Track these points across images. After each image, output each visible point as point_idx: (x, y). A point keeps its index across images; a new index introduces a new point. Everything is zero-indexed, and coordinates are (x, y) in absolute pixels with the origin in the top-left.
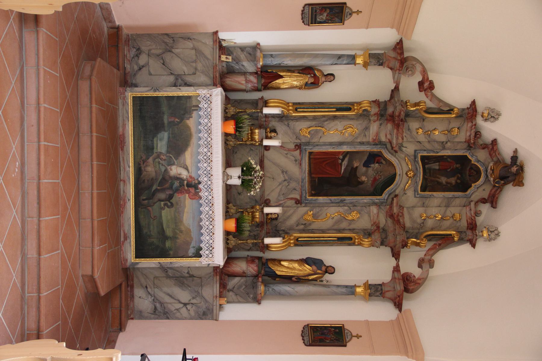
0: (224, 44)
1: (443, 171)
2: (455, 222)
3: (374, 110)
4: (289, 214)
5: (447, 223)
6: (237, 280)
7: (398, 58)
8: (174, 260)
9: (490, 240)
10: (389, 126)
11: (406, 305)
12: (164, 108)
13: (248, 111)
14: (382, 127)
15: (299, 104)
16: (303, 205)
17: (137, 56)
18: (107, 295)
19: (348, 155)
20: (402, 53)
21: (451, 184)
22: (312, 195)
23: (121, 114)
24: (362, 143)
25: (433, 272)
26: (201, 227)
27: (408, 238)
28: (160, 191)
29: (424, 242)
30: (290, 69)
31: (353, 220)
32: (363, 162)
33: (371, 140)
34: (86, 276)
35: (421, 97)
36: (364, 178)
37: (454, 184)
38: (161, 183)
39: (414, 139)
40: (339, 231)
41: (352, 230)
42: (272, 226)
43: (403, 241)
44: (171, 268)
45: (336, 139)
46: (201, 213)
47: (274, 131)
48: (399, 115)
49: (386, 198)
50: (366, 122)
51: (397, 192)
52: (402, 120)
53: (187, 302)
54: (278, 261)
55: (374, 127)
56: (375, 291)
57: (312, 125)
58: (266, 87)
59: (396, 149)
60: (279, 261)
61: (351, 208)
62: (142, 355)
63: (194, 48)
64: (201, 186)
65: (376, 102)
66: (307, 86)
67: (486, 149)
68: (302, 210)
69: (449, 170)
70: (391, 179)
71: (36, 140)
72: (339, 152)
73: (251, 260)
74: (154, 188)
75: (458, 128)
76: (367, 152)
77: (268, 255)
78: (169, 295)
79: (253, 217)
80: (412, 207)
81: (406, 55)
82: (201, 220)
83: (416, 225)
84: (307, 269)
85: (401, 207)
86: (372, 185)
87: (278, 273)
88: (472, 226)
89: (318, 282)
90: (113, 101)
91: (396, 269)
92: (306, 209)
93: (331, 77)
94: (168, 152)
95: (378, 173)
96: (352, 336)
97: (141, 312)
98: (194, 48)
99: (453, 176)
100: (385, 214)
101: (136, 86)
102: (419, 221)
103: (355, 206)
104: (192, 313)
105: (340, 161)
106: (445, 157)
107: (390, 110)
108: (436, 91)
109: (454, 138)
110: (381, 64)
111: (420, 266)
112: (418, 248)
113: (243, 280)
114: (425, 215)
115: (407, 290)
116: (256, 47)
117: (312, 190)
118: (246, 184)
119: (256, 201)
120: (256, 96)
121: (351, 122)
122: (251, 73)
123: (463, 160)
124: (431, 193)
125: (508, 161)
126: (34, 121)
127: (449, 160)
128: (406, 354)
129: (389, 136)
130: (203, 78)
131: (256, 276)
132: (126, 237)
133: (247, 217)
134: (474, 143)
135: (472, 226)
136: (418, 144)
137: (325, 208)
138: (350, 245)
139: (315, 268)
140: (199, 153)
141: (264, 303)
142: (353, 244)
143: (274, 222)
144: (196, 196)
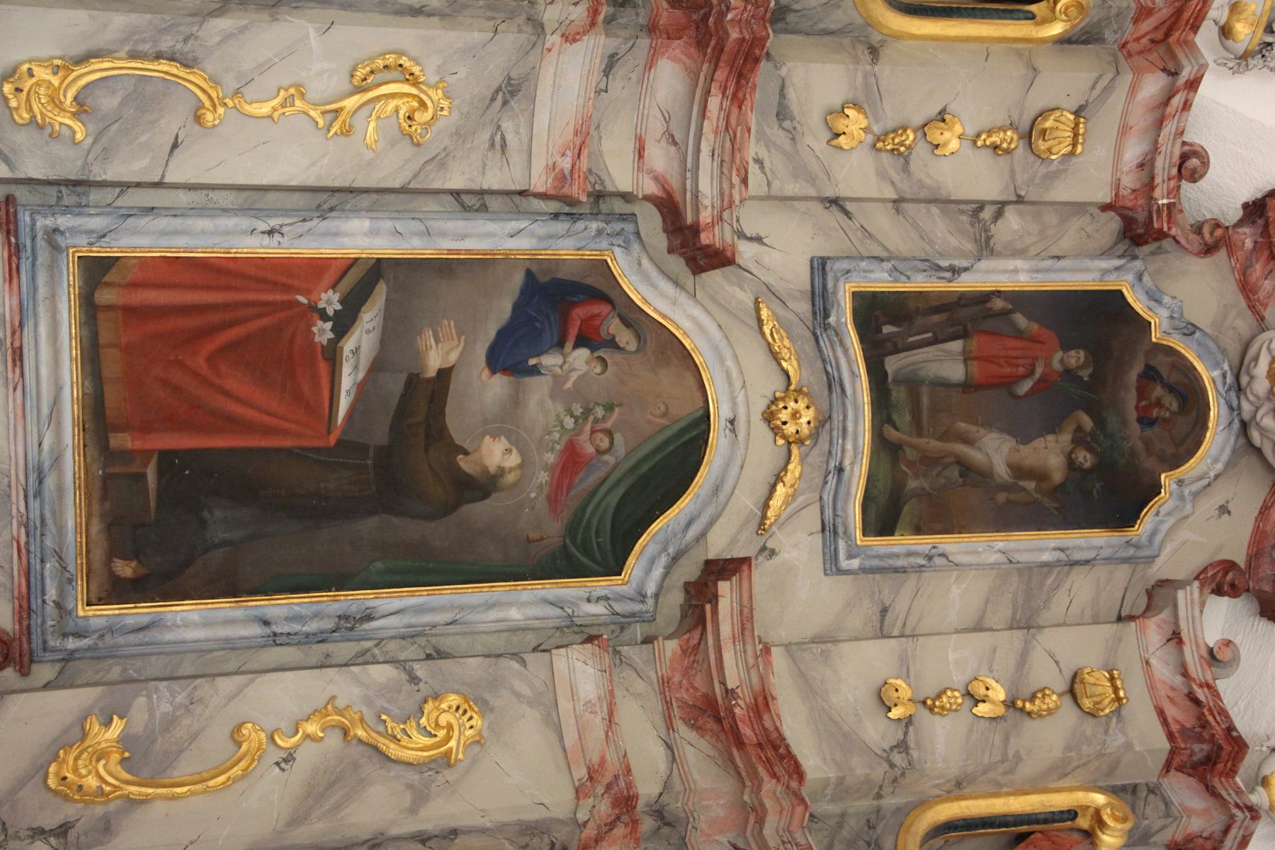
1: (988, 392)
2: (1089, 726)
10: (669, 77)
14: (617, 83)
16: (44, 672)
19: (381, 290)
21: (1040, 476)
22: (118, 591)
24: (472, 202)
31: (446, 761)
32: (490, 332)
36: (496, 454)
37: (1058, 477)
39: (812, 180)
45: (296, 161)
49: (651, 588)
50: (511, 39)
57: (101, 41)
61: (420, 670)
67: (1223, 253)
69: (1025, 387)
70: (674, 463)
72: (317, 267)
75: (1077, 113)
80: (819, 639)
83: (860, 768)
86: (553, 500)
92: (65, 704)
95: (588, 411)
99: (1052, 428)
100: (656, 704)
102: (877, 733)
103: (440, 654)
105: (323, 332)
106: (998, 304)
109: (1051, 177)
114: (905, 692)
117: (114, 552)
123: (1099, 320)
124: (923, 543)
127: (1021, 320)
129: (660, 158)
135: (1200, 750)
136: (832, 218)
137: (226, 685)
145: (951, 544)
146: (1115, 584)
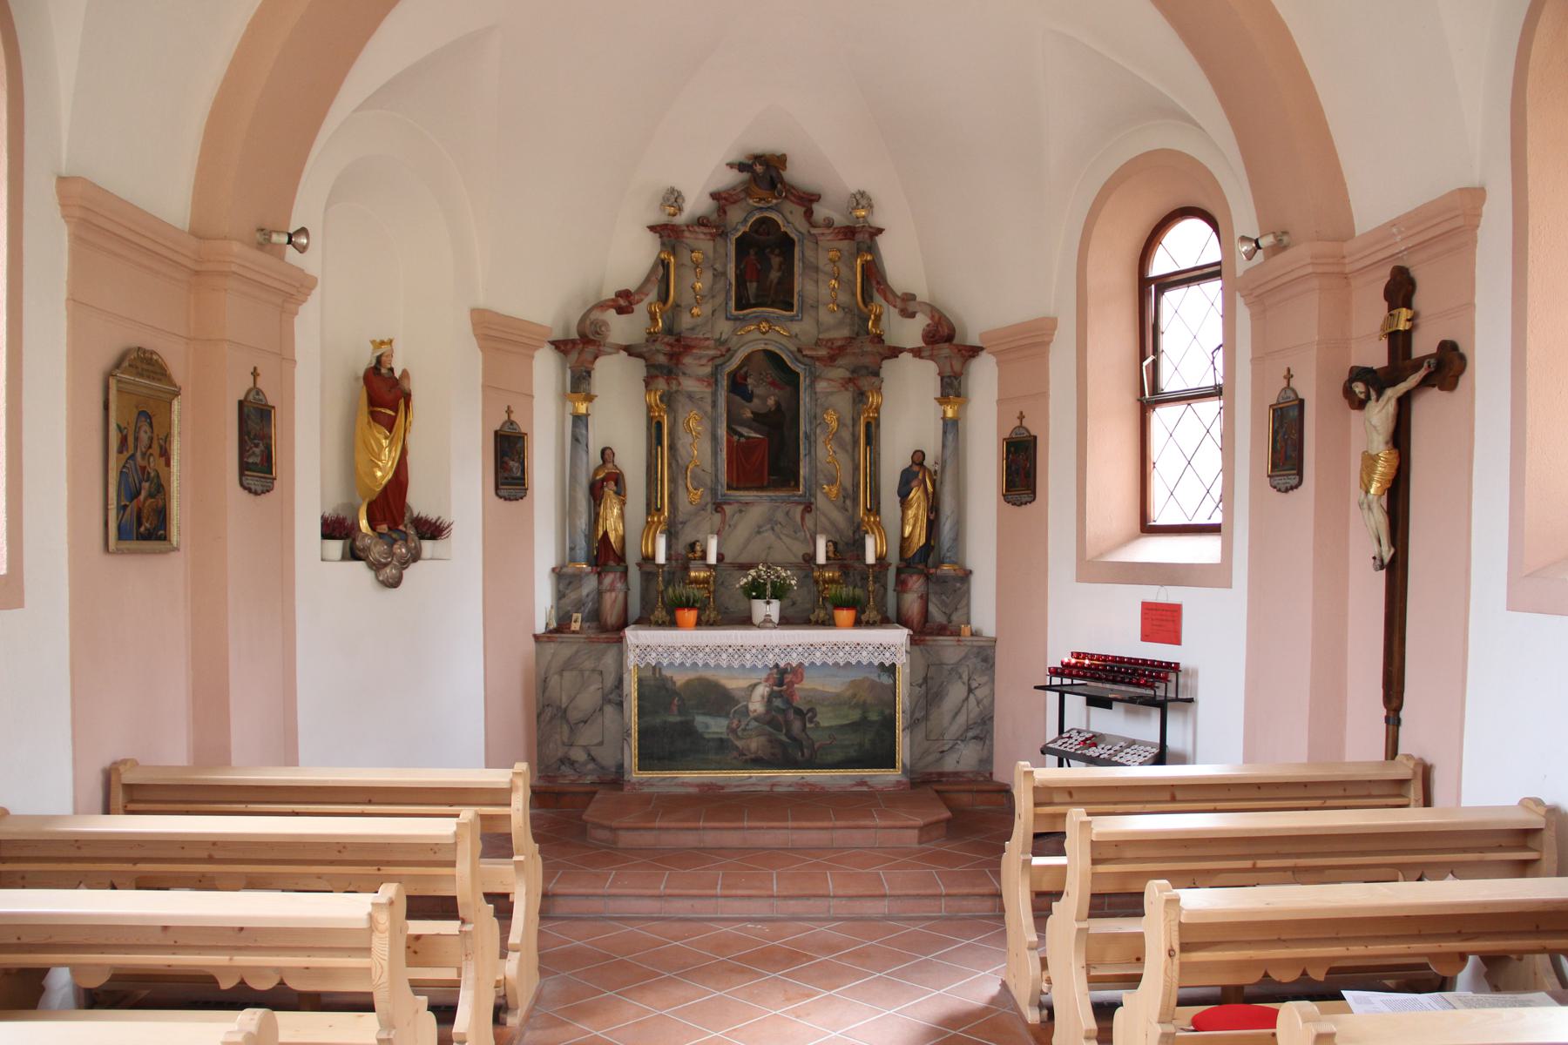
0: (554, 625)
3: (661, 384)
4: (827, 524)
5: (845, 271)
6: (932, 609)
7: (579, 348)
8: (899, 708)
9: (871, 206)
10: (687, 360)
11: (973, 340)
12: (657, 721)
13: (661, 587)
15: (648, 505)
17: (572, 763)
18: (950, 808)
20: (573, 342)
23: (667, 790)
24: (714, 405)
25: (922, 294)
26: (848, 664)
27: (868, 333)
28: (788, 724)
29: (875, 309)
30: (595, 519)
31: (838, 420)
33: (709, 390)
34: (920, 836)
35: (641, 309)
36: (771, 402)
38: (778, 728)
40: (856, 442)
41: (855, 422)
42: (847, 550)
43: (871, 341)
44: (912, 713)
45: (707, 446)
46: (824, 664)
47: (692, 546)
48: (671, 345)
51: (794, 349)
52: (678, 341)
53: (965, 689)
54: (904, 542)
55: (689, 385)
56: (952, 388)
58: (621, 559)
59: (723, 349)
60: (903, 539)
62: (1043, 753)
63: (561, 673)
64: (782, 664)
65: (648, 382)
66: (620, 492)
68: (821, 501)
70: (773, 357)
71: (713, 901)
72: (729, 441)
73: (901, 586)
74: (784, 738)
76: (729, 404)
77: (894, 558)
78: (955, 717)
79: (832, 581)
81: (574, 335)
82: (836, 664)
84: (916, 494)
85: (818, 343)
87: (923, 541)
88: (849, 232)
89: (938, 478)
90: (647, 800)
91: (917, 353)
92: (819, 495)
93: (607, 454)
94: (727, 716)
96: (1021, 426)
97: (981, 761)
98: (561, 673)
101: (621, 767)
102: (840, 314)
104: (985, 679)
107: (662, 359)
108: (631, 284)
110: (589, 373)
111: (912, 315)
112: (884, 318)
113: (933, 598)
115: (949, 338)
116: (558, 574)
118: (779, 591)
119: (806, 576)
120: (634, 575)
121: (680, 421)
122: (600, 582)
123: (743, 245)
125: (745, 176)
126: (687, 903)
128: (1047, 343)
129: (704, 361)
130: (609, 660)
131: (928, 577)
132: (862, 783)
133: (833, 590)
134: (717, 227)
138: (878, 426)
139: (914, 483)
140: (730, 667)
141: (970, 565)
142: (877, 420)
143: (840, 547)
144: (798, 671)
145: (797, 289)
146: (808, 244)
